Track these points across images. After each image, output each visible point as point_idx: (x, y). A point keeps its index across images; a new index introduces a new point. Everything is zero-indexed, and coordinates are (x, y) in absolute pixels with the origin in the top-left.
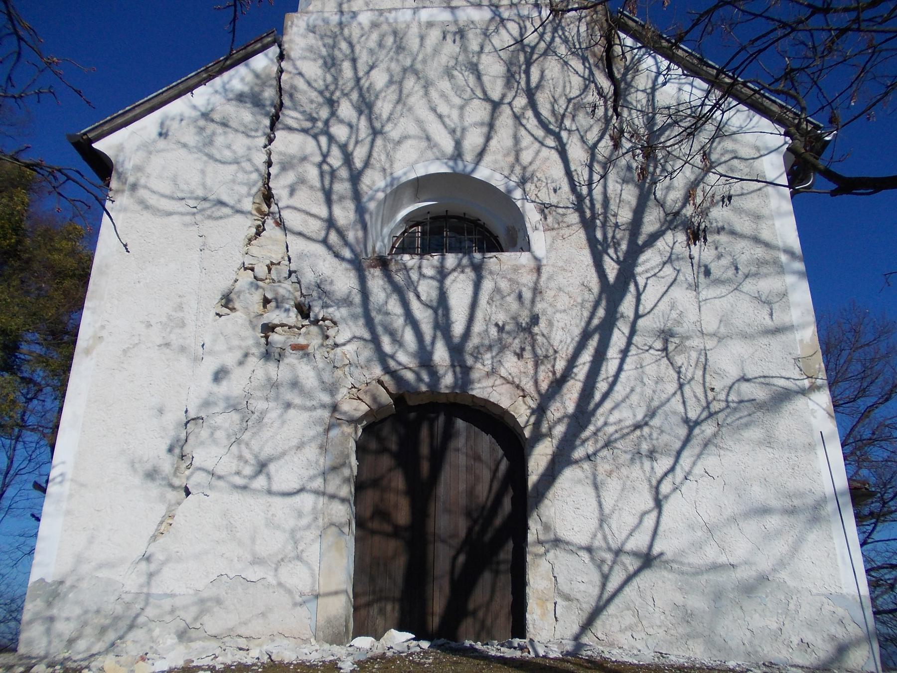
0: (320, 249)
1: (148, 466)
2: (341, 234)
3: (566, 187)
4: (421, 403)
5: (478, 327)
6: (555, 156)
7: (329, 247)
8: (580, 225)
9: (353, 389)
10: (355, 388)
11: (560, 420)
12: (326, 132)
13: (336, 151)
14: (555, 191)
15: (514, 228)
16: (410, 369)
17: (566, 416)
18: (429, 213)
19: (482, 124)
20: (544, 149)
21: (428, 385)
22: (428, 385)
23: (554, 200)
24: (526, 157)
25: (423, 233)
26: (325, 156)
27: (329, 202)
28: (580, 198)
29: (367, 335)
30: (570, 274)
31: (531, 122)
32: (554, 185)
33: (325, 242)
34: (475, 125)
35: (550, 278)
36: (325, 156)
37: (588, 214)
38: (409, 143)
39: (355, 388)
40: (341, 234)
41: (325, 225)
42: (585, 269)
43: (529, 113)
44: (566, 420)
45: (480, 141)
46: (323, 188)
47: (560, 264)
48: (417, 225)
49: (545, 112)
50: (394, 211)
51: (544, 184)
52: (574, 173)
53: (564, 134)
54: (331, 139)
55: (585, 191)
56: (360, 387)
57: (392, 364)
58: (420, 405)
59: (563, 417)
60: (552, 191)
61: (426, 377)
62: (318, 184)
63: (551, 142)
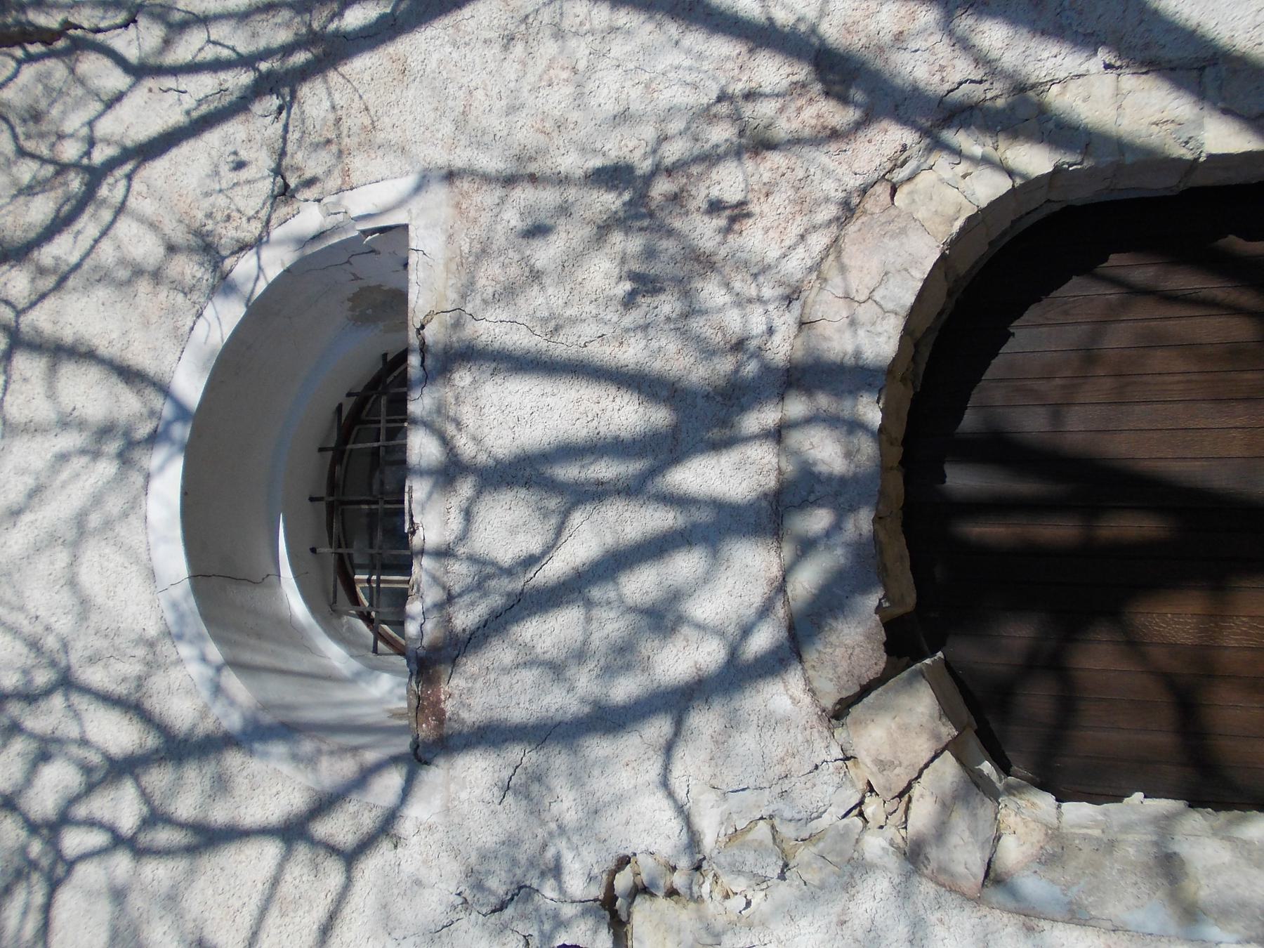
0: (372, 867)
1: (444, 172)
2: (324, 804)
3: (235, 130)
4: (907, 564)
5: (631, 353)
6: (157, 169)
7: (365, 845)
8: (333, 76)
9: (869, 810)
10: (861, 803)
11: (964, 44)
12: (52, 829)
13: (103, 805)
14: (240, 165)
15: (356, 298)
16: (787, 573)
17: (947, 26)
18: (313, 550)
19: (53, 370)
20: (132, 202)
21: (843, 510)
22: (843, 510)
23: (262, 162)
24: (145, 248)
25: (371, 569)
26: (119, 841)
27: (233, 834)
28: (264, 86)
29: (658, 728)
30: (480, 94)
31: (62, 249)
32: (225, 169)
33: (351, 857)
34: (52, 394)
35: (479, 141)
36: (119, 841)
37: (300, 58)
38: (89, 577)
39: (861, 803)
40: (324, 804)
41: (302, 851)
42: (463, 50)
43: (49, 254)
44: (965, 23)
45: (92, 374)
46: (191, 851)
47: (447, 128)
48: (350, 586)
49: (41, 209)
50: (288, 632)
51: (221, 201)
52: (195, 115)
53: (100, 155)
54: (64, 820)
55: (245, 78)
56: (862, 785)
57: (762, 640)
58: (914, 569)
59: (951, 33)
60: (244, 174)
61: (818, 520)
62: (179, 866)
63: (111, 190)
